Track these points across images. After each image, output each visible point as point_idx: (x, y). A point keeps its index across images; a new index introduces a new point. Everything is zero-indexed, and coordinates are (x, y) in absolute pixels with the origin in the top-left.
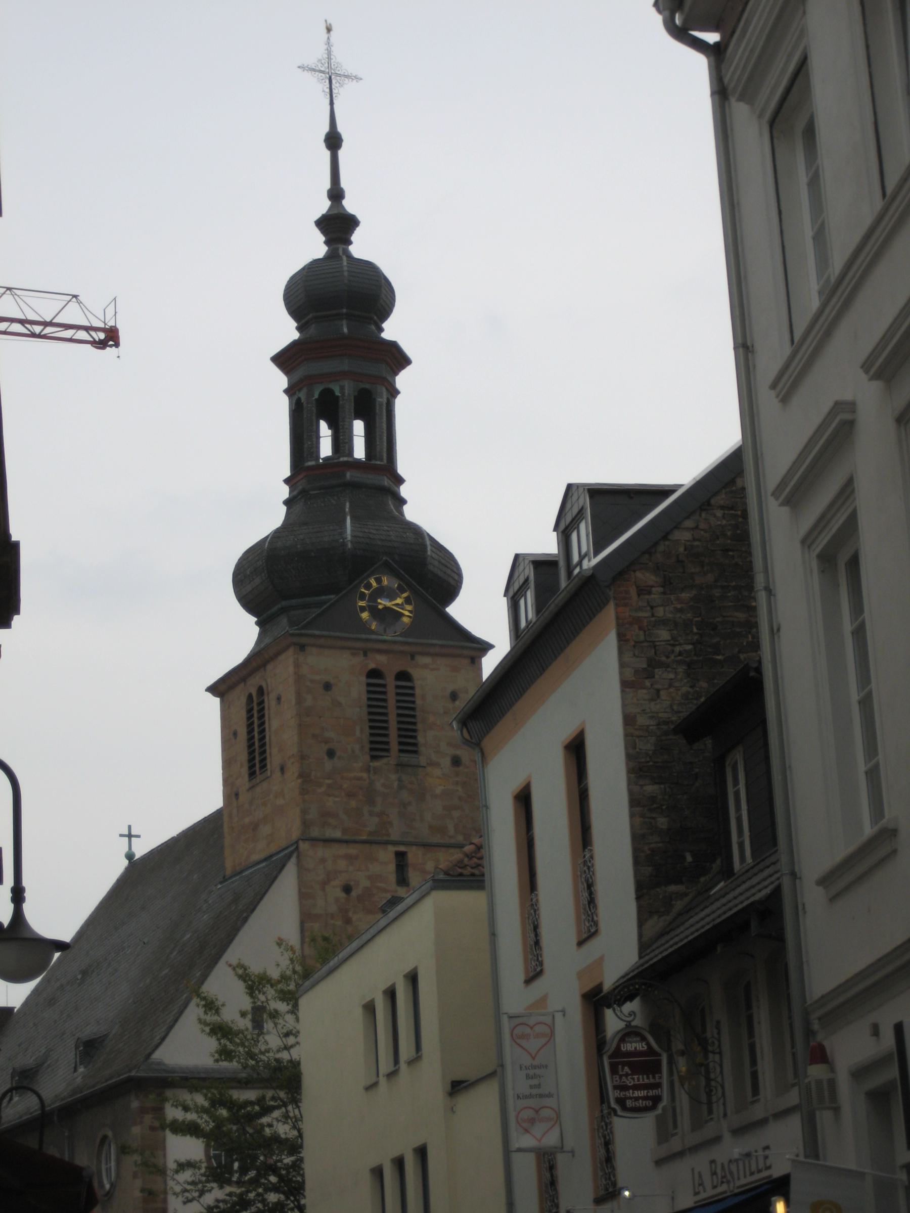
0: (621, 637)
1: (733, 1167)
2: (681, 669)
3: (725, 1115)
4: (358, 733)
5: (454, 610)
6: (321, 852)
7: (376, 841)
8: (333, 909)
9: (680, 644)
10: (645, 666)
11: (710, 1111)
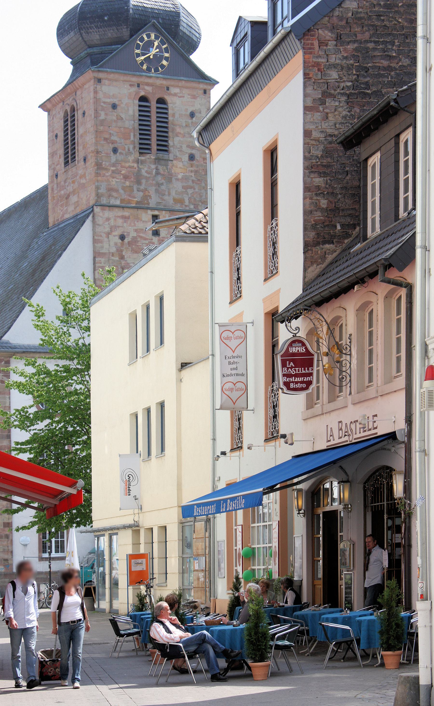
0: (306, 76)
1: (353, 426)
2: (344, 99)
3: (350, 393)
4: (132, 138)
5: (194, 57)
6: (107, 213)
7: (141, 206)
8: (113, 250)
9: (344, 81)
10: (320, 97)
11: (341, 391)
